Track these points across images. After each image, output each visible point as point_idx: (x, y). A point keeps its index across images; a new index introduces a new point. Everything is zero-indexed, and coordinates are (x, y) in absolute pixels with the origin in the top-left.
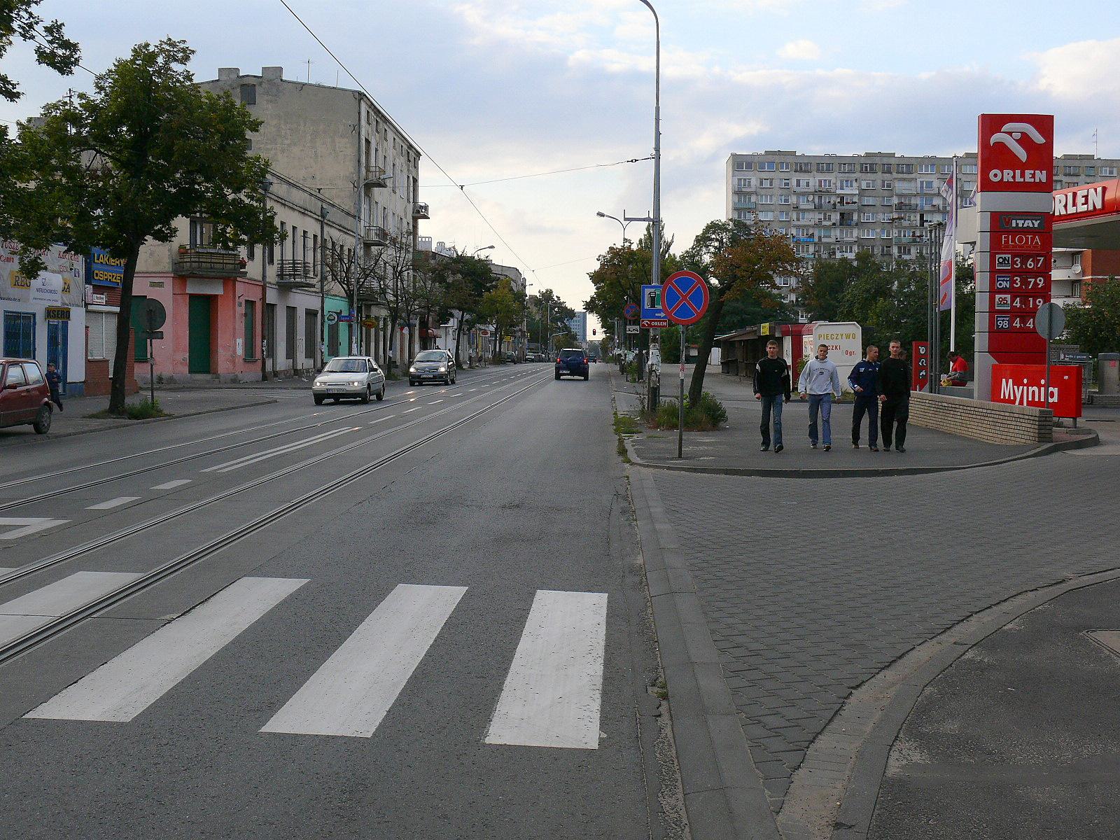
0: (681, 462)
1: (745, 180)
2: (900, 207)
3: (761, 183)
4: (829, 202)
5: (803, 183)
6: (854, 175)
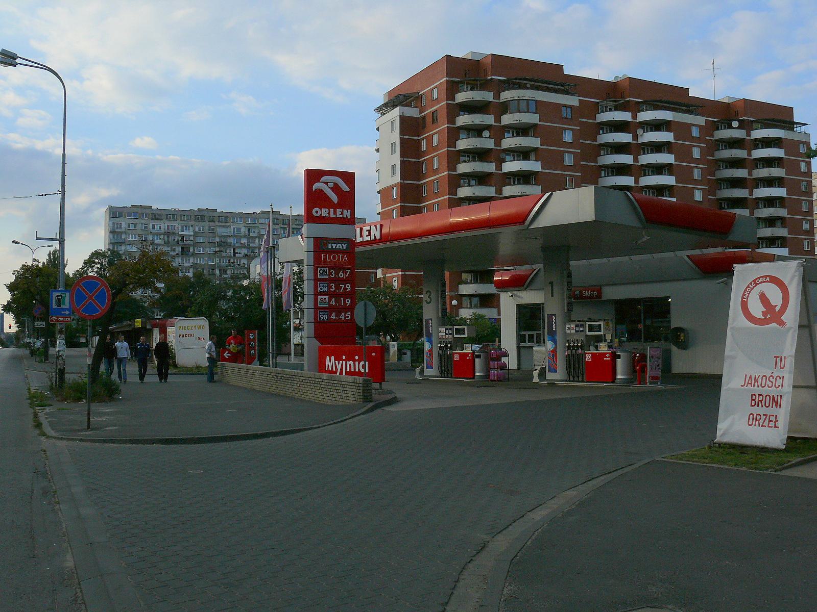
0: (90, 433)
1: (117, 223)
2: (220, 244)
3: (129, 227)
4: (174, 240)
5: (157, 227)
6: (190, 223)
